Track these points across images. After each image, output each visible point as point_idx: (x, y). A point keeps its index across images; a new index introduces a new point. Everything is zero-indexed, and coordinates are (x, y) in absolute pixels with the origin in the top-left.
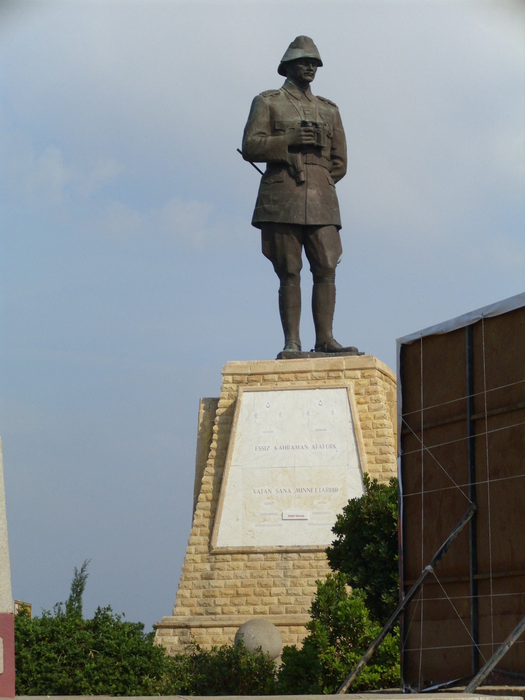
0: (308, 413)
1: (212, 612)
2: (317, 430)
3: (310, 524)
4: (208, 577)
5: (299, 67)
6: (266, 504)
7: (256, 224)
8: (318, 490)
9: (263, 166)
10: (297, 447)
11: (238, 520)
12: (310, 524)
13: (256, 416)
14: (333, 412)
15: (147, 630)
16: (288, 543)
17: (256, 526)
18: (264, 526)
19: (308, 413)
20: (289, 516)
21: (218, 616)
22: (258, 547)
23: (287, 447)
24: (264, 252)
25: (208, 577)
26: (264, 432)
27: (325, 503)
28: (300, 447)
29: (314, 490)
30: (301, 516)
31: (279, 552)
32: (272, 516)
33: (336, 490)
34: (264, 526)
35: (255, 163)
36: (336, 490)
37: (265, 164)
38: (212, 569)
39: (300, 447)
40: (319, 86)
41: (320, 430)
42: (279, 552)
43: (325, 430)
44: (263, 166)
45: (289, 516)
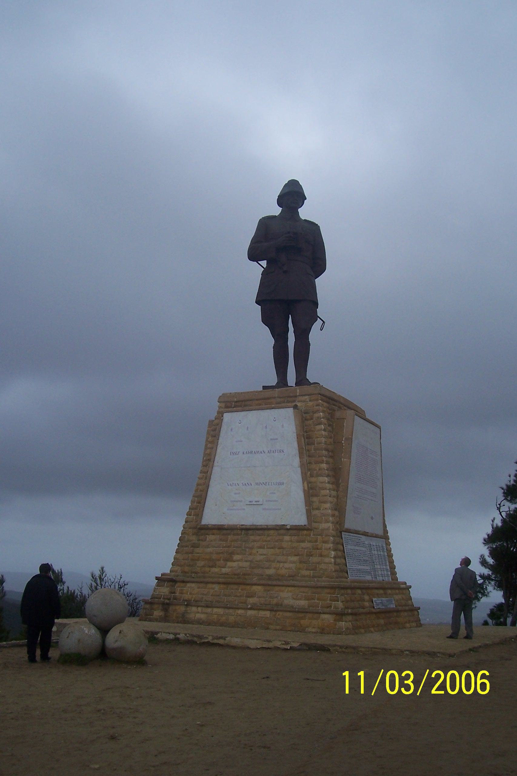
0: (266, 427)
2: (271, 439)
3: (264, 509)
4: (195, 546)
6: (236, 494)
7: (257, 302)
8: (270, 484)
9: (264, 263)
10: (258, 452)
12: (264, 509)
13: (232, 430)
14: (283, 426)
15: (509, 484)
17: (228, 510)
18: (232, 509)
19: (266, 427)
20: (256, 502)
21: (199, 574)
23: (251, 452)
25: (195, 546)
26: (236, 442)
27: (274, 493)
29: (267, 483)
31: (242, 529)
33: (281, 484)
34: (232, 509)
36: (281, 484)
38: (199, 540)
40: (304, 213)
41: (274, 439)
43: (277, 439)
44: (264, 263)
45: (256, 502)
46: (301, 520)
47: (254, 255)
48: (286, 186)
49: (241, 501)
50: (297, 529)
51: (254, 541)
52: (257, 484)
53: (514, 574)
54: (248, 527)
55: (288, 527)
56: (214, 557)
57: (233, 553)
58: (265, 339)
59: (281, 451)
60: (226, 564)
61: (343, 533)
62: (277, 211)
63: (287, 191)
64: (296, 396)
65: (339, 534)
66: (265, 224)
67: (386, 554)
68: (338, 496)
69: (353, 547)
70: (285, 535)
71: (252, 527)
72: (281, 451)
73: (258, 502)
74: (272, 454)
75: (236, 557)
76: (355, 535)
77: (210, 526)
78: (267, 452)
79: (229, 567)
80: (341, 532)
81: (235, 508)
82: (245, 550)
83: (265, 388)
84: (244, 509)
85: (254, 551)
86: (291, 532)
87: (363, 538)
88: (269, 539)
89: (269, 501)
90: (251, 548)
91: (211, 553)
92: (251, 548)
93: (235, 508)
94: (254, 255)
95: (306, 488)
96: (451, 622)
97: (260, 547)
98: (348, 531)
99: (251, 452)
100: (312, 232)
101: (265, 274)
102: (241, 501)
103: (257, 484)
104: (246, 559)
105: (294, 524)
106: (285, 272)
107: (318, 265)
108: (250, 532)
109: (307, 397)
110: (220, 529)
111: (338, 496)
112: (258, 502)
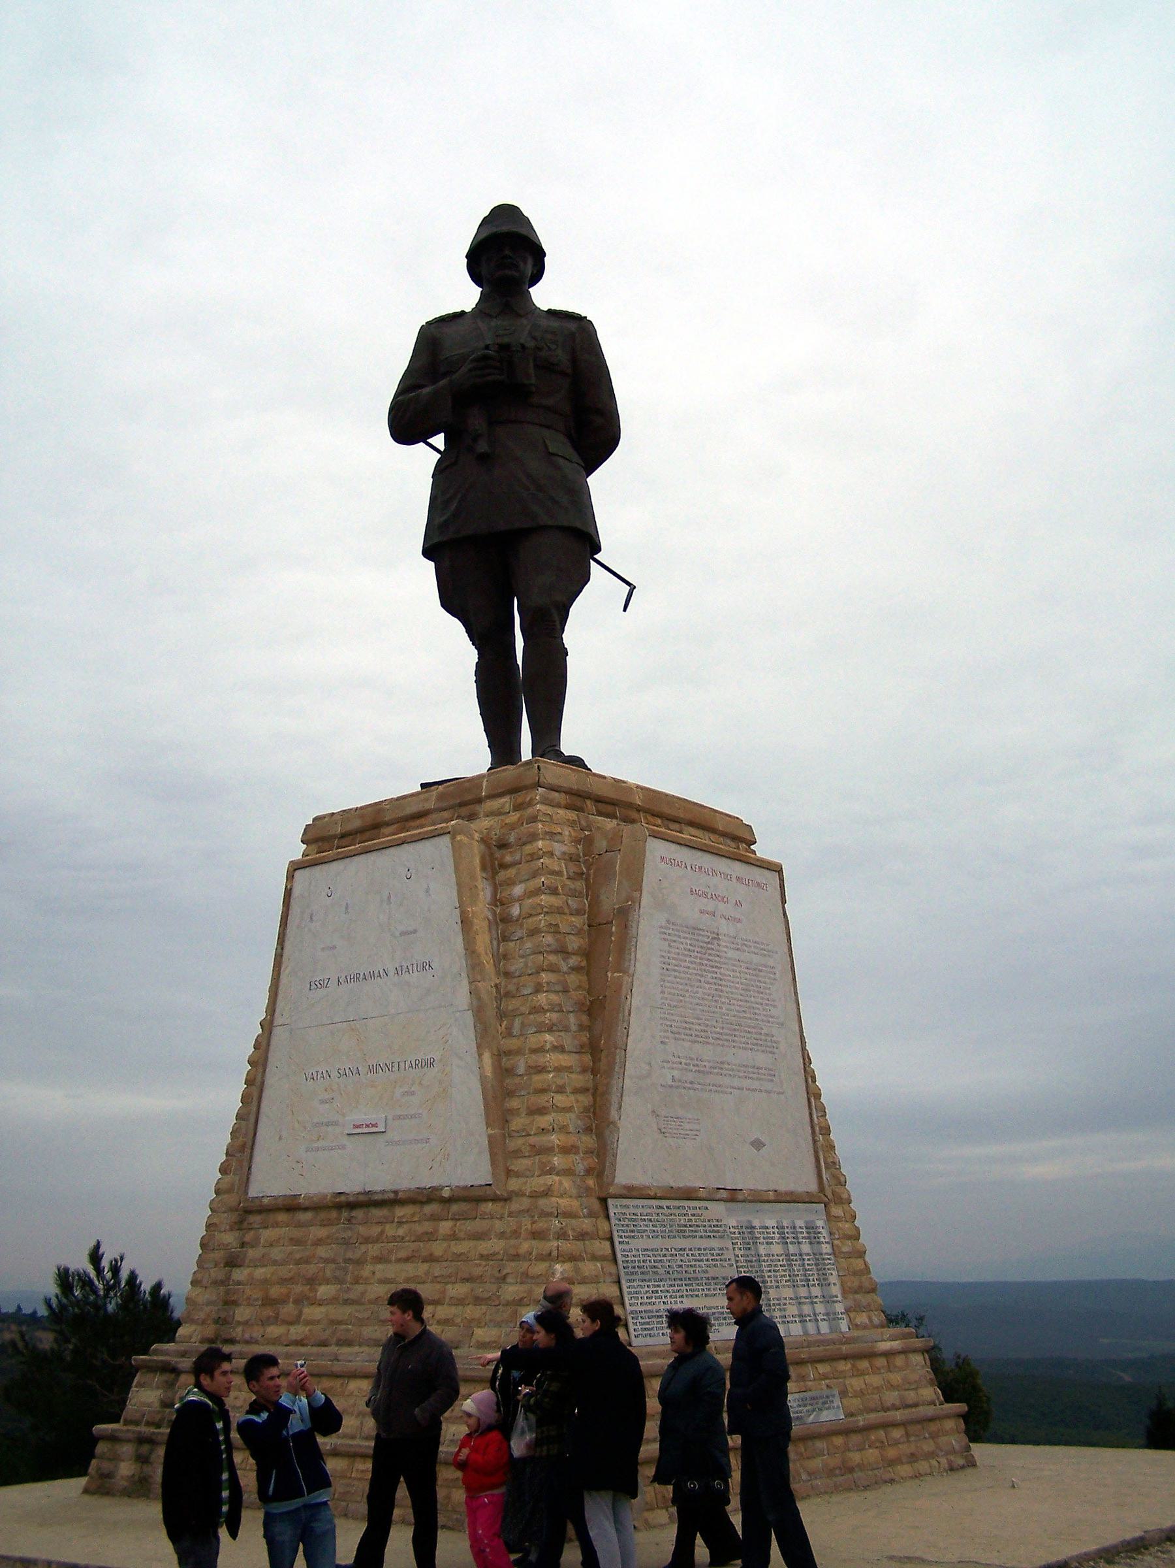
0: (389, 898)
1: (228, 1337)
2: (403, 934)
5: (506, 251)
6: (323, 1102)
8: (402, 1065)
9: (439, 440)
10: (372, 975)
11: (280, 1138)
14: (427, 890)
16: (352, 1183)
18: (318, 1149)
19: (389, 898)
22: (307, 1197)
23: (356, 978)
24: (445, 605)
27: (413, 1093)
28: (376, 974)
30: (367, 1126)
31: (339, 1207)
32: (330, 1129)
33: (430, 1063)
34: (318, 1149)
35: (429, 441)
36: (430, 1063)
37: (441, 436)
39: (376, 974)
42: (339, 1207)
43: (415, 931)
44: (439, 440)
46: (473, 1169)
47: (407, 424)
48: (485, 222)
49: (336, 1123)
50: (471, 1197)
51: (367, 1240)
52: (371, 1069)
53: (265, 1415)
54: (351, 1199)
55: (446, 1193)
56: (275, 1291)
57: (312, 1282)
58: (454, 650)
59: (427, 966)
60: (300, 1313)
61: (609, 1201)
62: (465, 296)
63: (483, 235)
64: (479, 801)
65: (596, 1205)
66: (435, 340)
67: (826, 1248)
68: (596, 1088)
69: (656, 1243)
70: (310, 1224)
71: (361, 1198)
72: (427, 966)
73: (375, 1125)
74: (406, 976)
75: (324, 1291)
76: (645, 1202)
77: (266, 1201)
78: (392, 973)
79: (308, 1323)
80: (604, 1201)
81: (320, 1144)
82: (345, 1270)
83: (423, 786)
84: (343, 1147)
85: (366, 1272)
86: (455, 1208)
87: (717, 1210)
88: (401, 1232)
89: (399, 1117)
90: (359, 1262)
91: (265, 1281)
92: (359, 1262)
93: (320, 1144)
94: (407, 424)
95: (489, 1073)
96: (801, 1506)
97: (380, 1259)
98: (632, 1193)
99: (356, 978)
100: (576, 336)
101: (440, 472)
102: (336, 1123)
103: (371, 1069)
104: (346, 1296)
105: (462, 1184)
106: (483, 458)
107: (594, 428)
108: (359, 1214)
109: (506, 799)
110: (291, 1206)
111: (596, 1088)
112: (375, 1125)
